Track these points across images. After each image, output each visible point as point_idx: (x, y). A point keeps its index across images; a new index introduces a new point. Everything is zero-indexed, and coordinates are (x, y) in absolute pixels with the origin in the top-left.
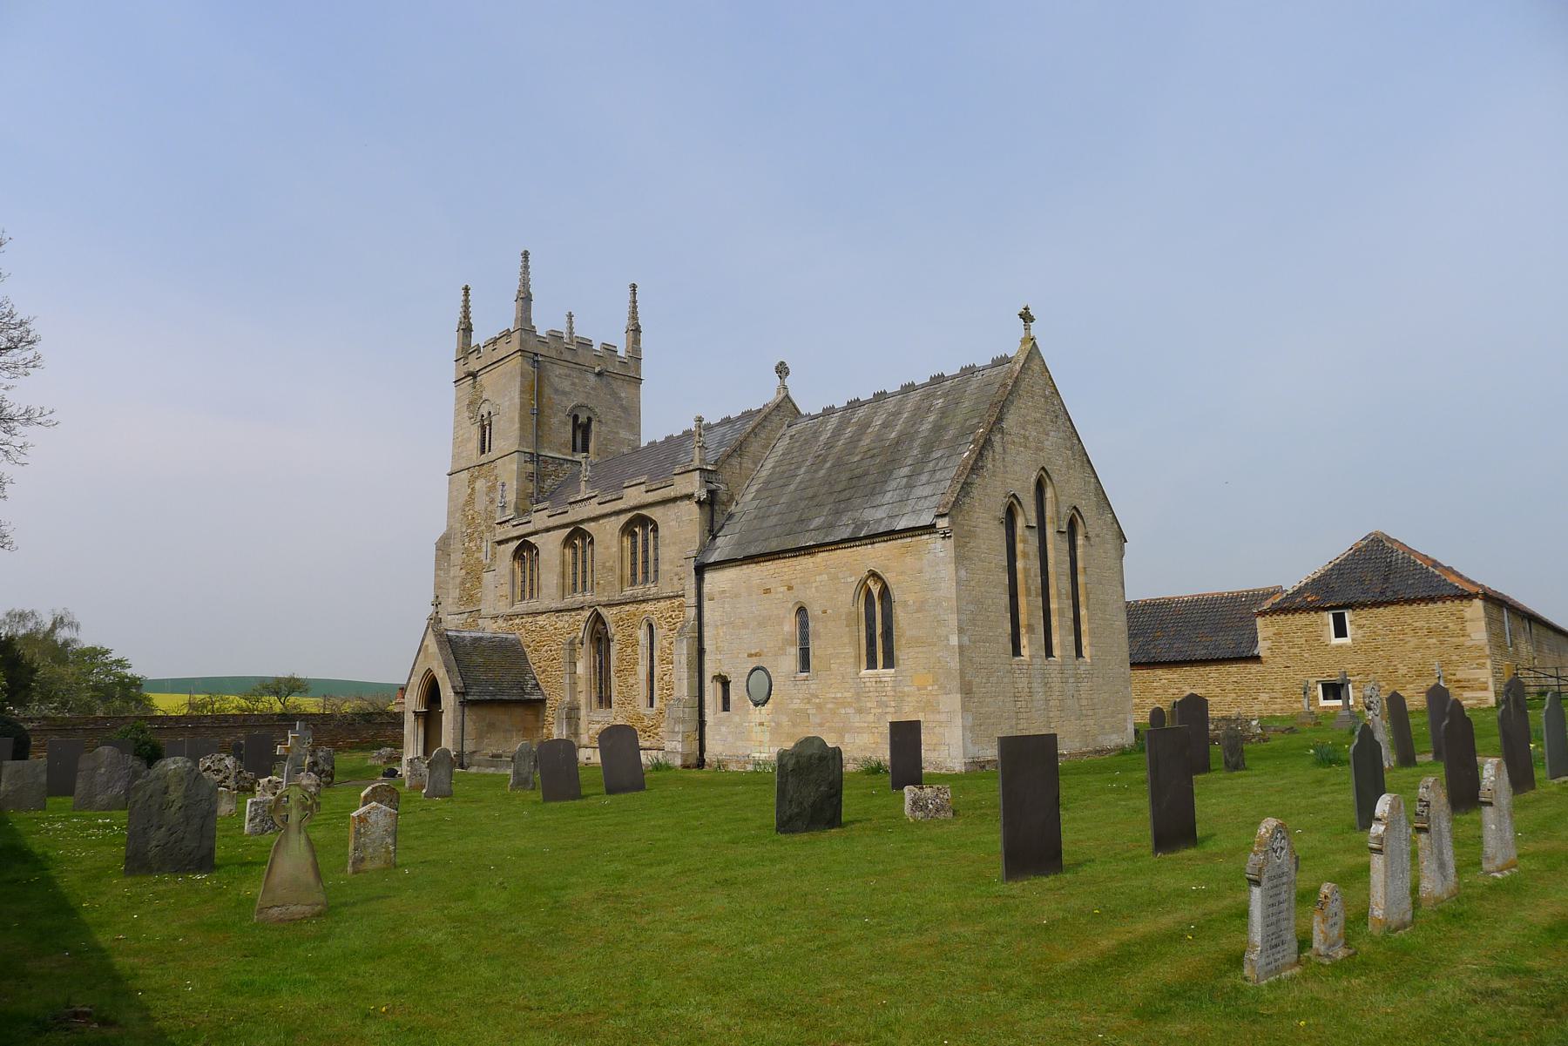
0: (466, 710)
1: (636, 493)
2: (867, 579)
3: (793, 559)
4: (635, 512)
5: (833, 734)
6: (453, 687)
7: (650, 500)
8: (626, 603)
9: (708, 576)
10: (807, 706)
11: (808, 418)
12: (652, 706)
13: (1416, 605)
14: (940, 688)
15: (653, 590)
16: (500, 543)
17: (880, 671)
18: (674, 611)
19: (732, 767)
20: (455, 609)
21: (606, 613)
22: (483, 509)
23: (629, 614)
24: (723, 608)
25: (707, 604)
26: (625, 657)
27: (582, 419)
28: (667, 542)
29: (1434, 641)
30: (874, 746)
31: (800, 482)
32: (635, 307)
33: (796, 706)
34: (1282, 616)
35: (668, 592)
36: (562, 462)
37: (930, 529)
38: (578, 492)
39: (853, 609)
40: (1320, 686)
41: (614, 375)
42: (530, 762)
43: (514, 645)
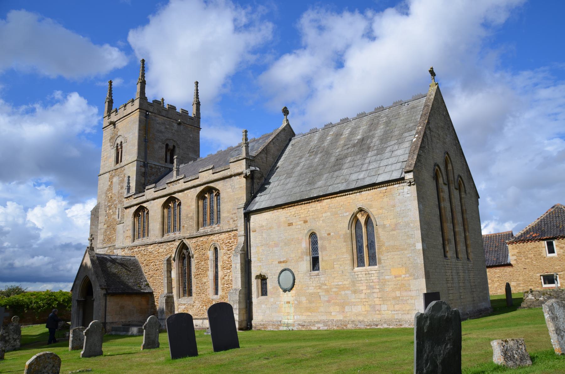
0: (108, 298)
1: (206, 175)
3: (307, 205)
4: (206, 185)
5: (336, 307)
6: (100, 286)
8: (201, 236)
9: (253, 218)
10: (319, 291)
11: (301, 136)
12: (216, 293)
14: (410, 276)
15: (216, 228)
16: (126, 208)
17: (367, 267)
18: (231, 239)
19: (270, 328)
21: (189, 243)
22: (117, 192)
23: (204, 243)
24: (262, 236)
26: (200, 267)
27: (171, 147)
30: (366, 313)
31: (304, 165)
32: (197, 93)
33: (311, 291)
34: (521, 244)
35: (226, 228)
36: (160, 167)
37: (401, 180)
38: (172, 177)
40: (542, 277)
41: (187, 125)
42: (156, 330)
43: (134, 263)
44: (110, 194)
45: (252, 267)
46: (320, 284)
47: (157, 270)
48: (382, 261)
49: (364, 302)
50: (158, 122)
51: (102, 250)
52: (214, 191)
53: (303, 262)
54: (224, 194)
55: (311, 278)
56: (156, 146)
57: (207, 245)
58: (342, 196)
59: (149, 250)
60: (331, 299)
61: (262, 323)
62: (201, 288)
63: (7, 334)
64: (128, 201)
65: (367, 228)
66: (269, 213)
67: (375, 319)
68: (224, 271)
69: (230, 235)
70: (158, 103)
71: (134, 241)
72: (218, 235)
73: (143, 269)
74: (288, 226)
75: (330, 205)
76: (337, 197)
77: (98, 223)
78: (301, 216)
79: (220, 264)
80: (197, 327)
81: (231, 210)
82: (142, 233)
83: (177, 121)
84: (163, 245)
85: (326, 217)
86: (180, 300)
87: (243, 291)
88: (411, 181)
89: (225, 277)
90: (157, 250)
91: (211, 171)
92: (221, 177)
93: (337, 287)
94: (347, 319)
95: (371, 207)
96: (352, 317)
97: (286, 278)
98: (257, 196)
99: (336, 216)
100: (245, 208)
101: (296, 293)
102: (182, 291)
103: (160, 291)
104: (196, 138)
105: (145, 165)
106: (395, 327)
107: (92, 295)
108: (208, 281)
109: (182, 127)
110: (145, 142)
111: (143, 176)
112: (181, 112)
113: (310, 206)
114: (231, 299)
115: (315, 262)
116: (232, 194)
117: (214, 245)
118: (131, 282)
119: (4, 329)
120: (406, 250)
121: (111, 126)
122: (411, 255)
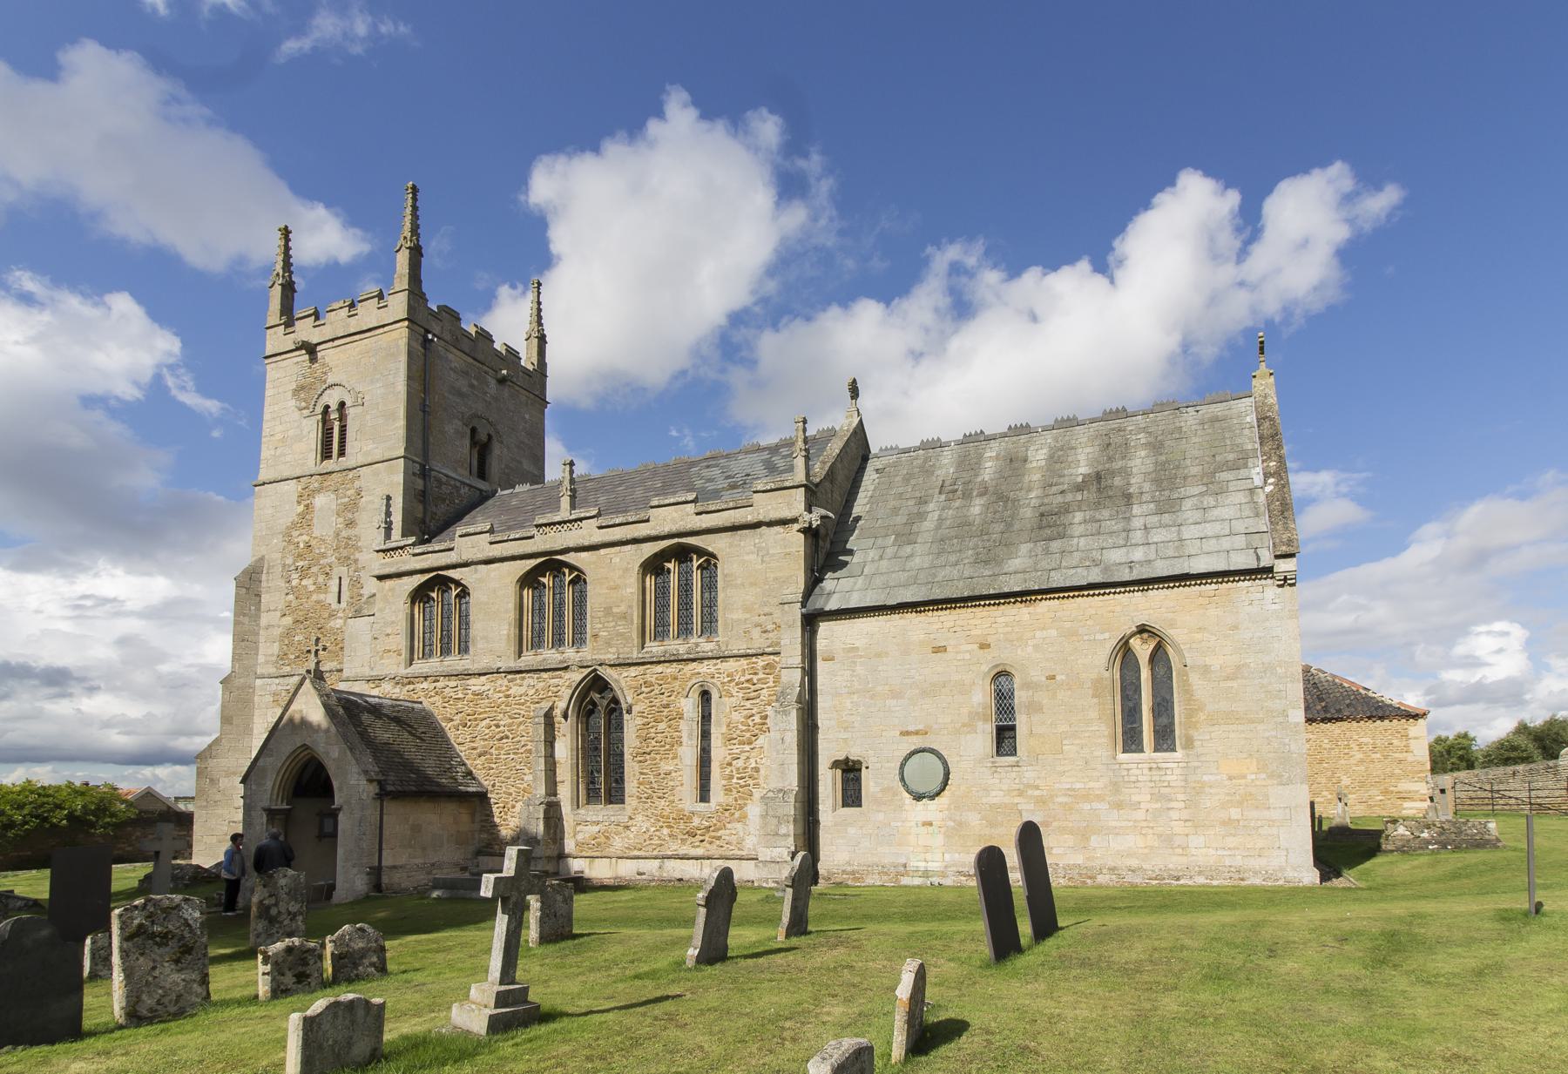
1: (675, 515)
2: (1130, 637)
4: (676, 540)
5: (1066, 836)
7: (704, 526)
8: (659, 662)
10: (1016, 800)
13: (1363, 722)
14: (1271, 776)
18: (756, 674)
20: (272, 670)
22: (331, 533)
23: (662, 677)
25: (821, 666)
27: (483, 437)
28: (739, 582)
29: (1378, 756)
30: (1146, 851)
33: (995, 801)
35: (738, 647)
36: (458, 484)
39: (1107, 674)
41: (517, 388)
44: (305, 538)
45: (819, 741)
46: (1022, 787)
47: (502, 739)
48: (1197, 743)
49: (1142, 827)
50: (453, 365)
51: (277, 681)
52: (695, 557)
53: (974, 735)
54: (734, 566)
55: (996, 772)
56: (450, 429)
57: (677, 683)
58: (1050, 599)
59: (474, 688)
60: (1050, 820)
61: (849, 869)
62: (655, 785)
63: (273, 901)
64: (387, 560)
65: (1151, 669)
66: (876, 620)
67: (1171, 866)
68: (729, 747)
69: (753, 663)
70: (453, 316)
71: (411, 664)
72: (714, 661)
73: (451, 735)
74: (933, 652)
75: (1058, 614)
76: (1078, 596)
77: (258, 609)
78: (972, 633)
79: (717, 733)
80: (644, 877)
81: (756, 606)
82: (439, 646)
83: (496, 372)
84: (524, 678)
85: (1044, 638)
86: (582, 811)
87: (800, 795)
88: (1288, 577)
89: (734, 762)
90: (504, 688)
91: (690, 508)
92: (729, 525)
93: (1069, 793)
94: (1097, 863)
95: (1172, 625)
96: (1110, 859)
97: (925, 772)
98: (824, 579)
99: (1074, 638)
100: (804, 605)
101: (950, 804)
102: (585, 792)
103: (514, 789)
104: (537, 424)
105: (424, 473)
106: (1226, 883)
107: (332, 796)
108: (679, 770)
109: (506, 392)
110: (424, 412)
111: (420, 501)
112: (504, 352)
113: (1000, 612)
114: (771, 813)
115: (1005, 737)
116: (760, 567)
117: (702, 686)
118: (430, 767)
119: (265, 886)
120: (1263, 721)
121: (297, 353)
122: (1274, 733)
